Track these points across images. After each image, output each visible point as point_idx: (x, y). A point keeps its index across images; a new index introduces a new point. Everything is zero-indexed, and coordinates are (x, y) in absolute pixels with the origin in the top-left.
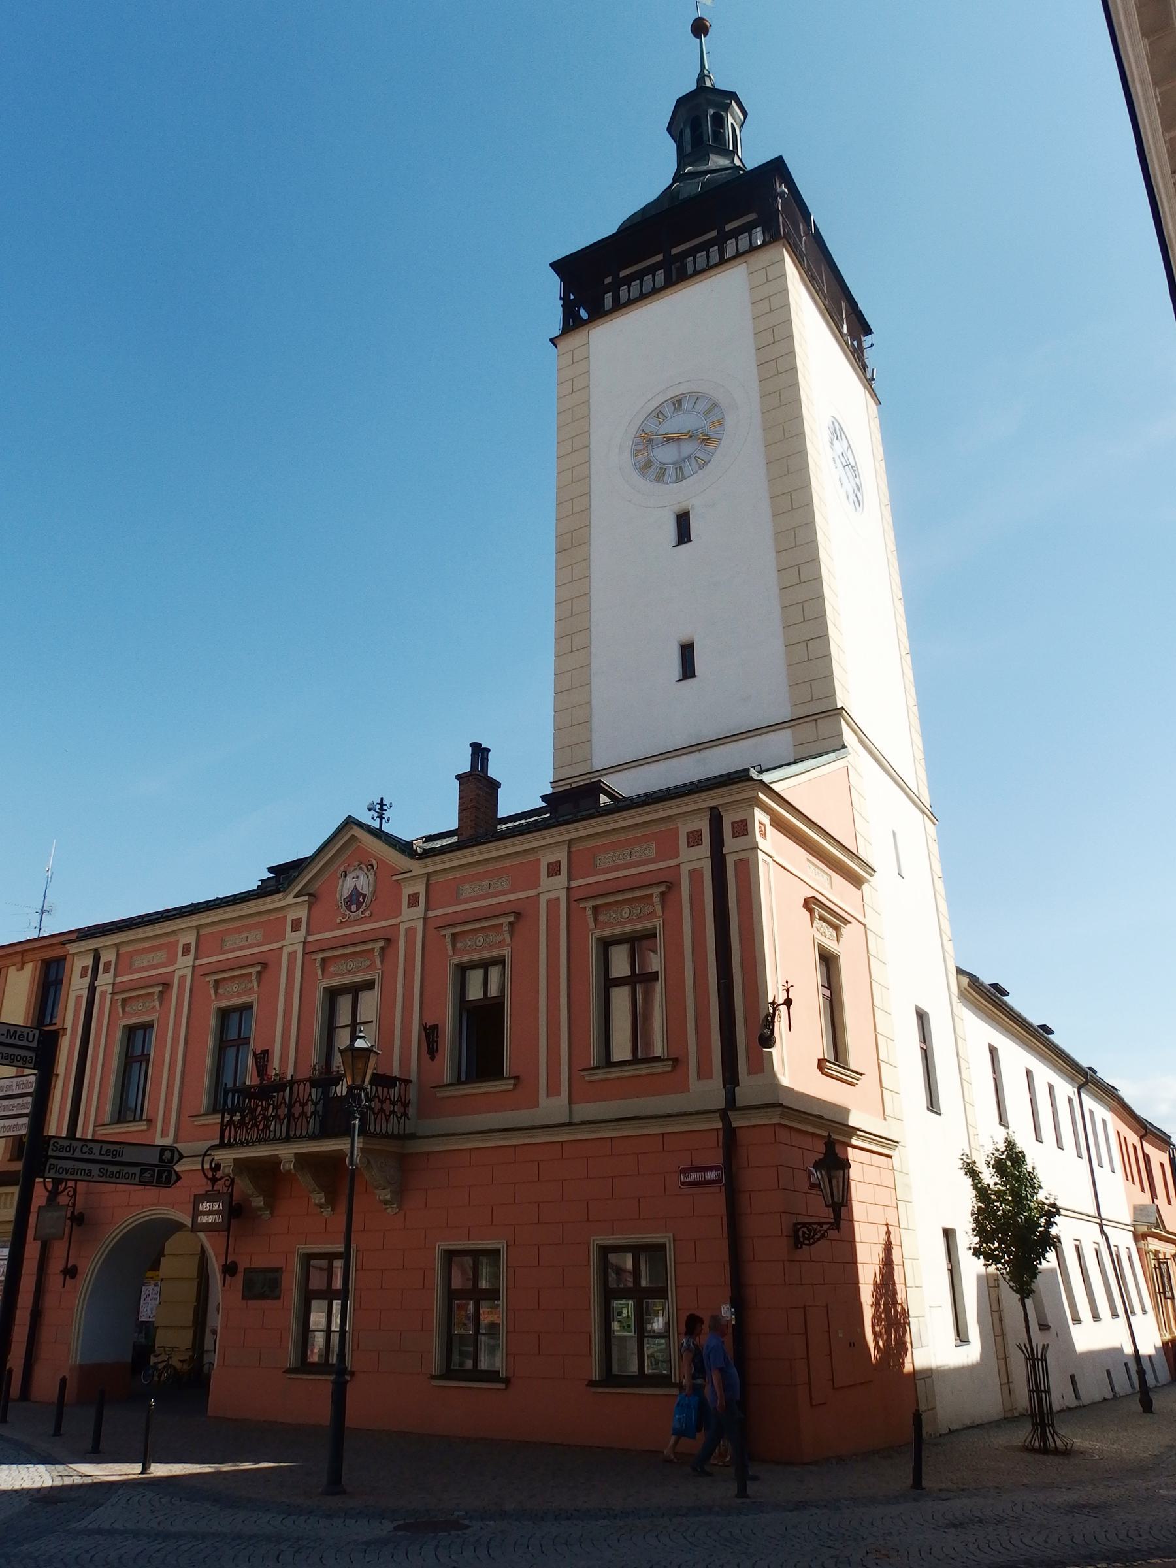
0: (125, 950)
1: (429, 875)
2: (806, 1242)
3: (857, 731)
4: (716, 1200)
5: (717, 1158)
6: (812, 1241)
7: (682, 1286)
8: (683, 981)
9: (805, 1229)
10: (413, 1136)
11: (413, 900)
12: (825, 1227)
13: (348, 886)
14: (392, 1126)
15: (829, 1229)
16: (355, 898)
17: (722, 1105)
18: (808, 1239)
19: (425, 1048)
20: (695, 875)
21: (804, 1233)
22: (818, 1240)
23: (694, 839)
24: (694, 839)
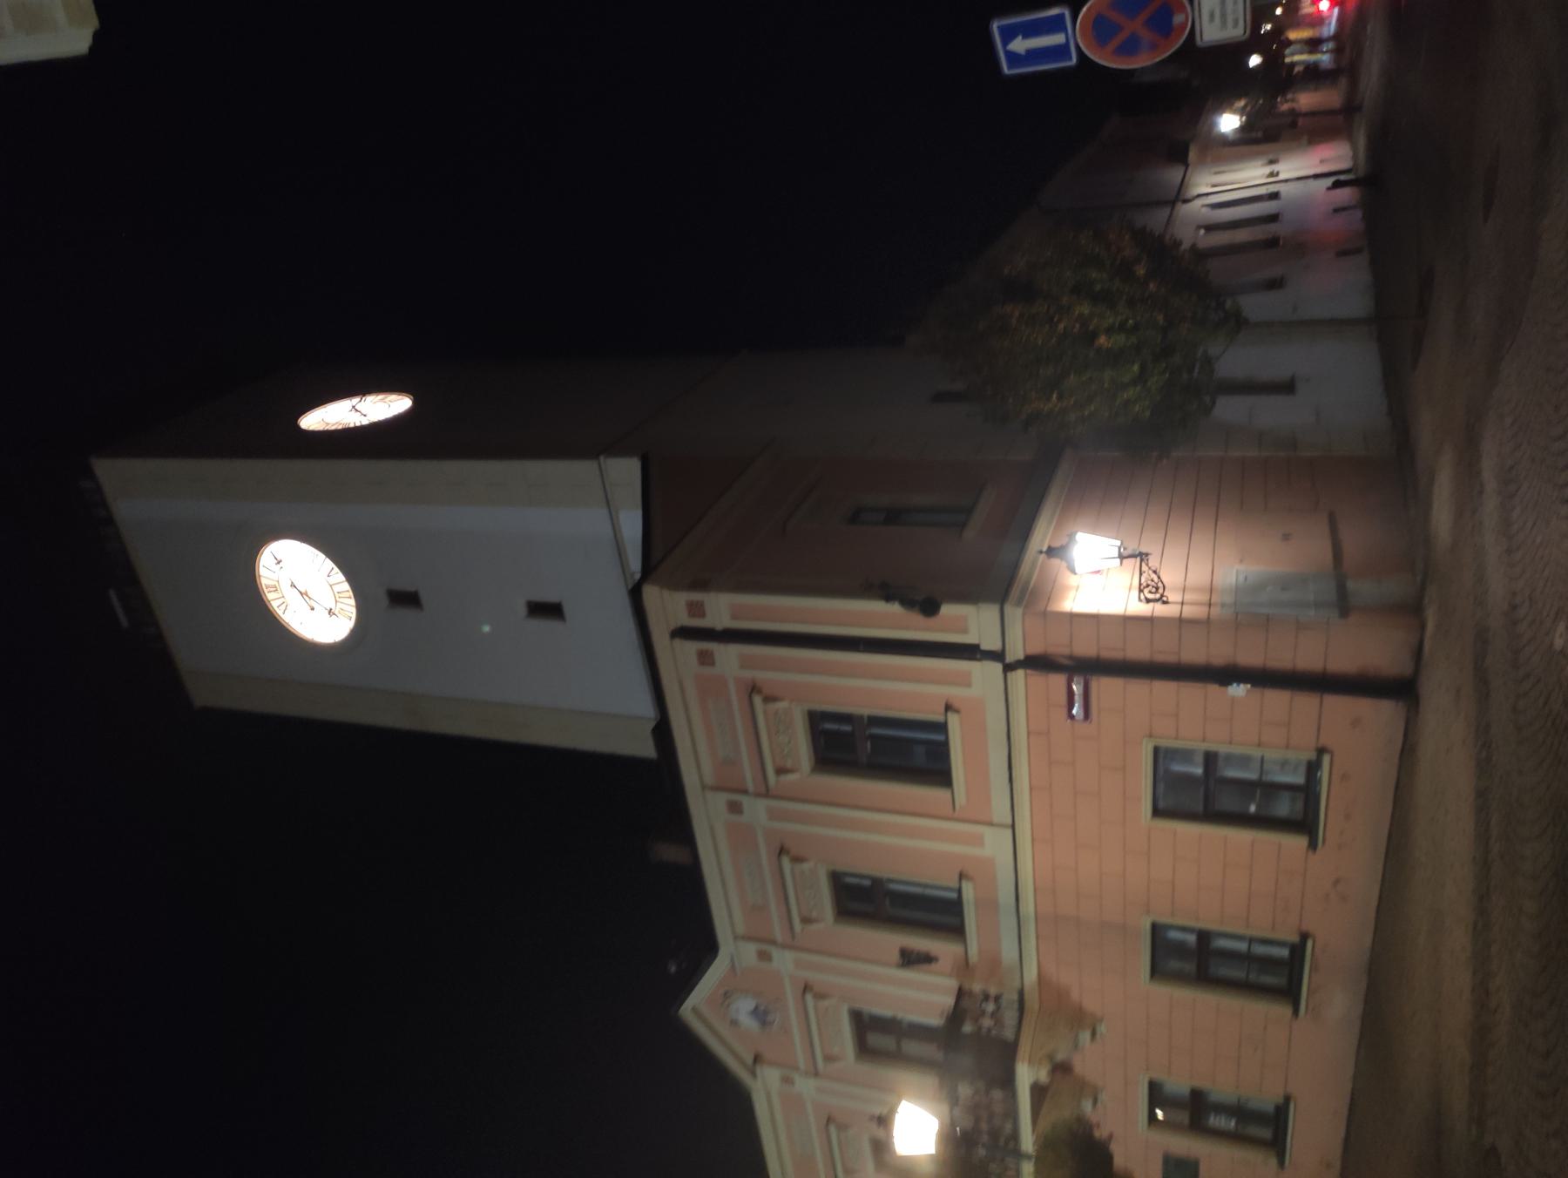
0: (740, 929)
1: (736, 938)
2: (1161, 591)
3: (627, 585)
4: (1106, 688)
5: (1058, 680)
6: (1160, 585)
7: (1204, 733)
8: (1041, 63)
9: (1146, 591)
10: (1021, 993)
11: (764, 956)
12: (1144, 568)
13: (748, 1023)
14: (1010, 1017)
15: (1147, 565)
16: (761, 1015)
17: (998, 667)
18: (1157, 589)
19: (925, 967)
20: (746, 663)
21: (1150, 592)
22: (1159, 578)
23: (705, 658)
24: (705, 658)
